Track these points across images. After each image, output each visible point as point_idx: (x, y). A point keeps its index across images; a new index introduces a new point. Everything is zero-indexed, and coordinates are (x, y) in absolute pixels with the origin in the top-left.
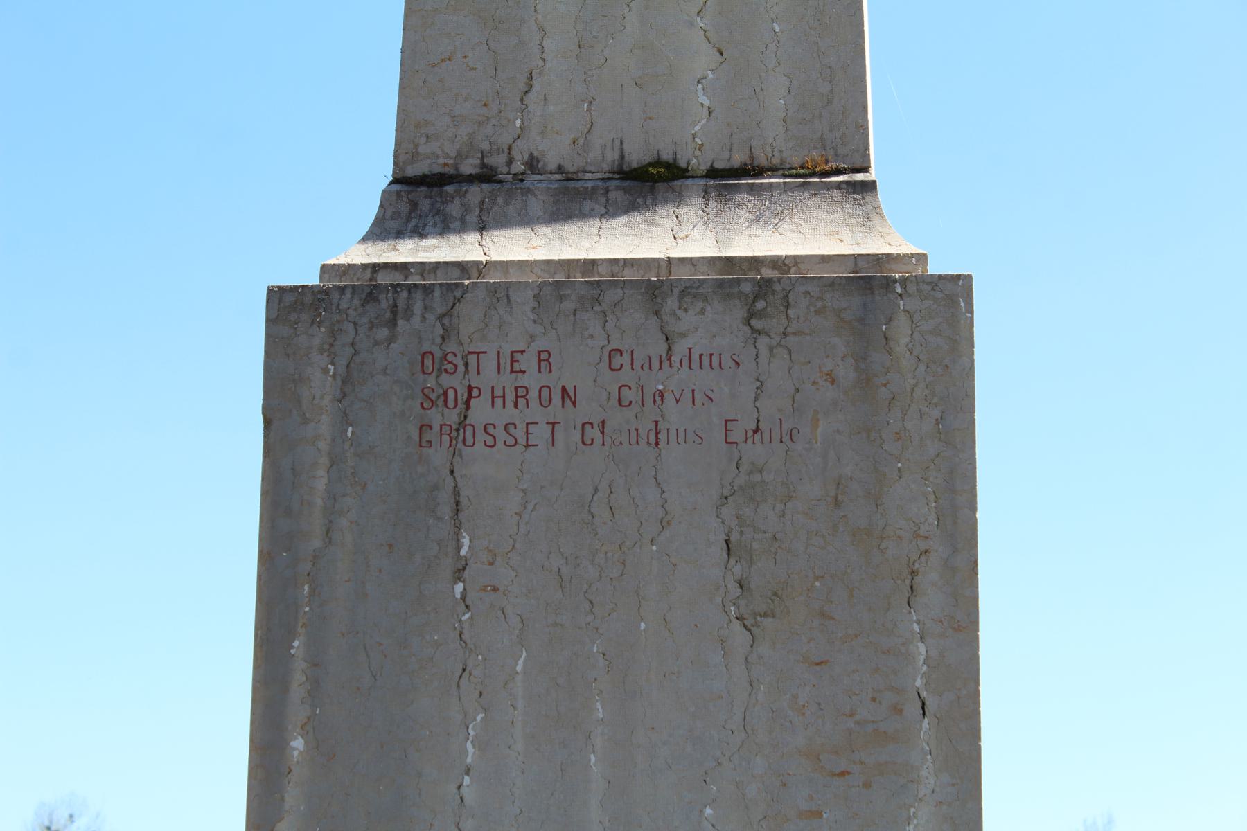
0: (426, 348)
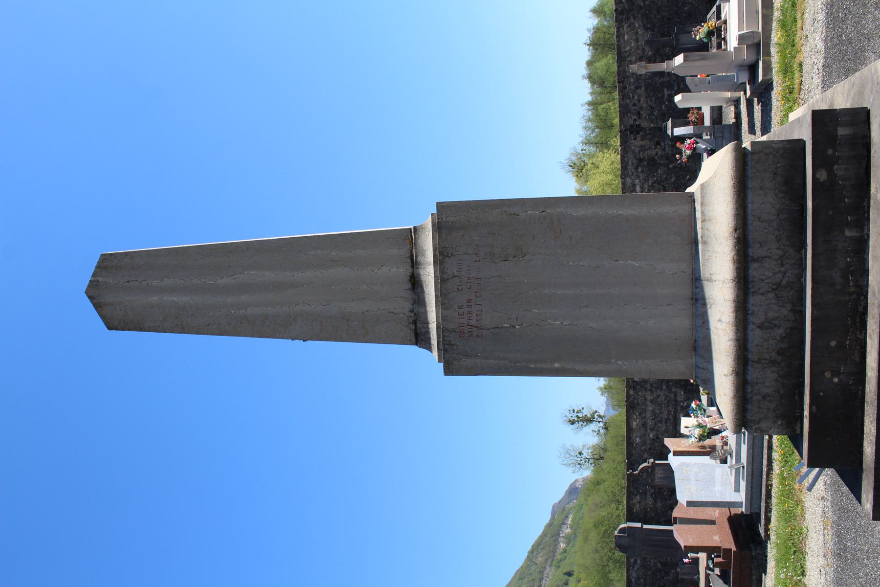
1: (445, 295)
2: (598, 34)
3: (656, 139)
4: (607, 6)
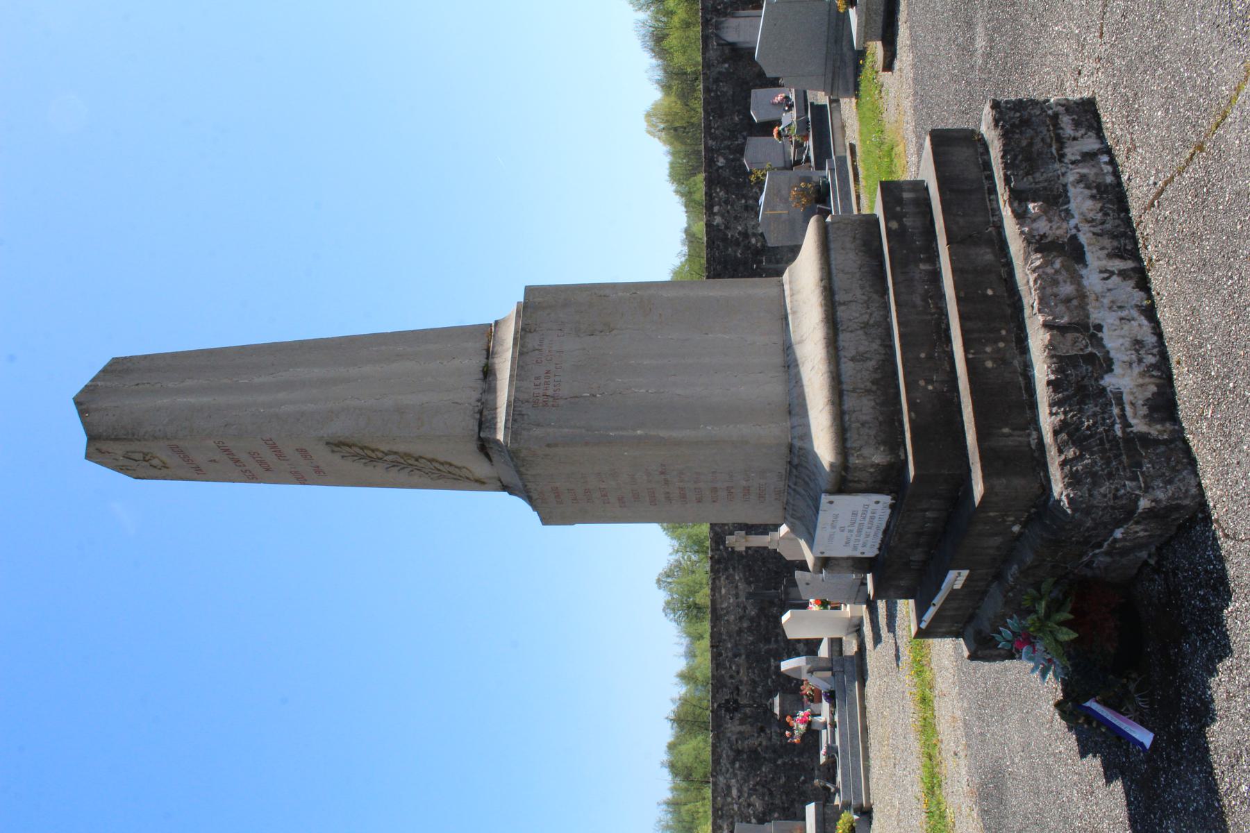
0: (531, 406)
1: (522, 367)
2: (685, 708)
3: (759, 724)
4: (699, 669)
